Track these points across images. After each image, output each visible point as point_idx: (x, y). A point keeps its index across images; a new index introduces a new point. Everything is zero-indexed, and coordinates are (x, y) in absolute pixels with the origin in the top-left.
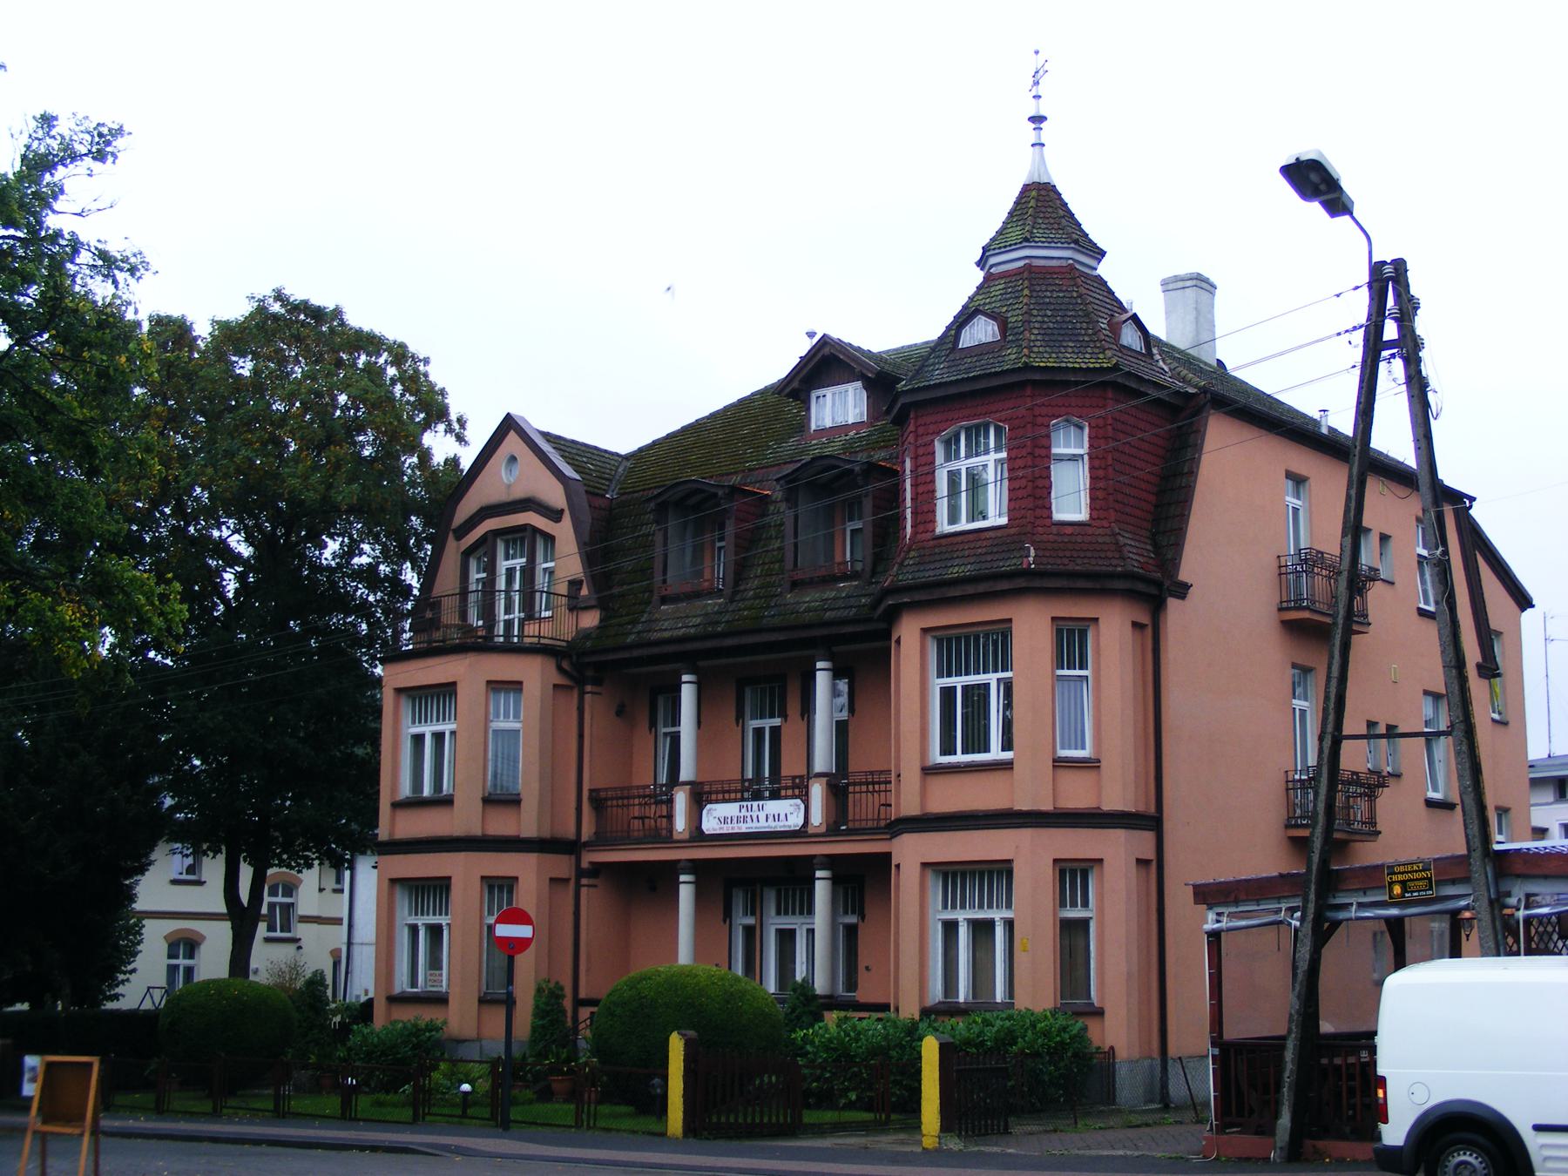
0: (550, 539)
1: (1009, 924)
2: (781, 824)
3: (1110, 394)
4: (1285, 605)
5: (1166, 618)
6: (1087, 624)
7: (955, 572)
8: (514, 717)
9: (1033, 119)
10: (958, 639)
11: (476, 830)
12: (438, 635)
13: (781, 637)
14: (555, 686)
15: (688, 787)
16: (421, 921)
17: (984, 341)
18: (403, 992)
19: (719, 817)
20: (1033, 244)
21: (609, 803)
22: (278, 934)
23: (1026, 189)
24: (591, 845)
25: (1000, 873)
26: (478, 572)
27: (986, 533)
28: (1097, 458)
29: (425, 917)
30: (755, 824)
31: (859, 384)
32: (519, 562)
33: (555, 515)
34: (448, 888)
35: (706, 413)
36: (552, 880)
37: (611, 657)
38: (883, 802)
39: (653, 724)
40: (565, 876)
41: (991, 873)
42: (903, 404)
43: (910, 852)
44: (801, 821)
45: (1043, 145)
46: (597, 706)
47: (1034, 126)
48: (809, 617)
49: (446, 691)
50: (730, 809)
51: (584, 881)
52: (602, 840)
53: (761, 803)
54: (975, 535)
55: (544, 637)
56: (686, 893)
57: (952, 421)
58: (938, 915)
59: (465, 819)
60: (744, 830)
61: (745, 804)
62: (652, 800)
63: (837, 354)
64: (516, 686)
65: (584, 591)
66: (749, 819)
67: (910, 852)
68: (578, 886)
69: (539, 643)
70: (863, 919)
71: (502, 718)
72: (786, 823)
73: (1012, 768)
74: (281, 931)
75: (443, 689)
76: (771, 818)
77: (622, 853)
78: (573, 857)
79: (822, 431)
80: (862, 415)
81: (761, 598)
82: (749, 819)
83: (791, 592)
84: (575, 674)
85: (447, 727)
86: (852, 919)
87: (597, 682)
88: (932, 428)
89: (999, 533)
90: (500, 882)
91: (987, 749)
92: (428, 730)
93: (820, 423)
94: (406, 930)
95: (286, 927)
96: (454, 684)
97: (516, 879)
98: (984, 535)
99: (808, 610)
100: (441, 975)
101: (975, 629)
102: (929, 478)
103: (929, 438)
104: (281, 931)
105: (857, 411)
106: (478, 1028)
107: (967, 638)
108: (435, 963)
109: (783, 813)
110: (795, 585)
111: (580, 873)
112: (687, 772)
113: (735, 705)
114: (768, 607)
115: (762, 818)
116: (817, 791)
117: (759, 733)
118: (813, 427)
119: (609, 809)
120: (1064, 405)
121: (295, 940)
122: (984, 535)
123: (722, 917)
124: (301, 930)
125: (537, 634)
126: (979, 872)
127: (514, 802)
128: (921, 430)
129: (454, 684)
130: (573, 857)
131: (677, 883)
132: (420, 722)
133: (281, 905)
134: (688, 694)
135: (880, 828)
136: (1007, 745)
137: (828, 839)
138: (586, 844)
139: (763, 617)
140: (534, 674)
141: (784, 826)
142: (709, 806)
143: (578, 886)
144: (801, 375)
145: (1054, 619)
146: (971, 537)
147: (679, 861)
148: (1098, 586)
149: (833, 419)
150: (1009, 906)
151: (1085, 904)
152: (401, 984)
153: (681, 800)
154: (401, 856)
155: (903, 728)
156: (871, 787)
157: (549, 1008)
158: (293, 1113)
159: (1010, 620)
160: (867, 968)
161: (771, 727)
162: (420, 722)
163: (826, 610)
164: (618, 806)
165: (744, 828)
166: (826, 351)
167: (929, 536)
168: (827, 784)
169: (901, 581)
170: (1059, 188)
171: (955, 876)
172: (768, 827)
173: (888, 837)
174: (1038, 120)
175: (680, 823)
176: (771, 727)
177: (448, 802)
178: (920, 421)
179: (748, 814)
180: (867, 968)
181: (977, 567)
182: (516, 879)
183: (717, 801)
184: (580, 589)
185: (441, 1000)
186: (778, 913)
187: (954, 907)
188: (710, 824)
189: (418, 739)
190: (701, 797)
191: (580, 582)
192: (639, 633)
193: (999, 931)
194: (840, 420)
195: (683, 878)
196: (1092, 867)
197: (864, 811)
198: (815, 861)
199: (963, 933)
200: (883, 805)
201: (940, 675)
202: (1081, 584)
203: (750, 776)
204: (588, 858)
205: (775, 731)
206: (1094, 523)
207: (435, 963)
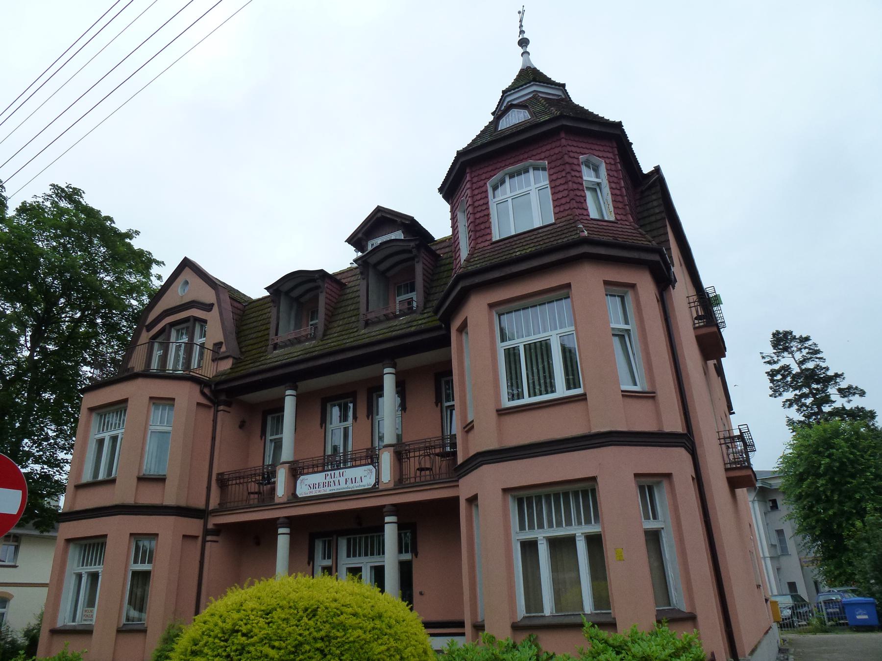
0: (204, 322)
2: (357, 484)
6: (626, 289)
11: (130, 500)
14: (198, 404)
16: (85, 570)
18: (64, 626)
21: (230, 483)
23: (522, 71)
24: (216, 512)
25: (585, 493)
29: (88, 567)
30: (337, 487)
32: (185, 339)
33: (208, 307)
34: (103, 545)
36: (185, 536)
39: (263, 433)
41: (566, 495)
42: (462, 162)
44: (372, 481)
46: (227, 420)
49: (120, 406)
50: (317, 478)
51: (209, 538)
52: (223, 509)
53: (341, 471)
56: (283, 541)
57: (496, 170)
60: (328, 492)
61: (329, 473)
64: (169, 401)
65: (223, 349)
66: (332, 484)
68: (204, 542)
70: (416, 556)
72: (361, 484)
77: (234, 516)
82: (332, 484)
83: (365, 328)
84: (212, 398)
85: (119, 432)
86: (407, 557)
87: (229, 404)
88: (483, 177)
91: (551, 388)
94: (74, 577)
103: (482, 183)
106: (114, 653)
108: (91, 603)
110: (367, 324)
111: (207, 532)
112: (287, 454)
115: (342, 480)
116: (386, 459)
119: (230, 487)
123: (307, 560)
126: (564, 493)
128: (475, 180)
131: (275, 535)
136: (572, 381)
142: (302, 477)
143: (204, 542)
147: (384, 506)
152: (64, 620)
154: (75, 522)
155: (415, 439)
160: (421, 593)
164: (236, 484)
165: (328, 491)
166: (379, 215)
175: (281, 491)
177: (110, 481)
178: (474, 174)
179: (332, 480)
180: (421, 593)
183: (308, 474)
184: (220, 348)
186: (348, 556)
187: (531, 527)
188: (303, 490)
189: (101, 442)
190: (296, 471)
191: (221, 343)
193: (581, 547)
195: (281, 531)
196: (659, 483)
198: (385, 510)
203: (330, 453)
204: (214, 521)
207: (91, 603)
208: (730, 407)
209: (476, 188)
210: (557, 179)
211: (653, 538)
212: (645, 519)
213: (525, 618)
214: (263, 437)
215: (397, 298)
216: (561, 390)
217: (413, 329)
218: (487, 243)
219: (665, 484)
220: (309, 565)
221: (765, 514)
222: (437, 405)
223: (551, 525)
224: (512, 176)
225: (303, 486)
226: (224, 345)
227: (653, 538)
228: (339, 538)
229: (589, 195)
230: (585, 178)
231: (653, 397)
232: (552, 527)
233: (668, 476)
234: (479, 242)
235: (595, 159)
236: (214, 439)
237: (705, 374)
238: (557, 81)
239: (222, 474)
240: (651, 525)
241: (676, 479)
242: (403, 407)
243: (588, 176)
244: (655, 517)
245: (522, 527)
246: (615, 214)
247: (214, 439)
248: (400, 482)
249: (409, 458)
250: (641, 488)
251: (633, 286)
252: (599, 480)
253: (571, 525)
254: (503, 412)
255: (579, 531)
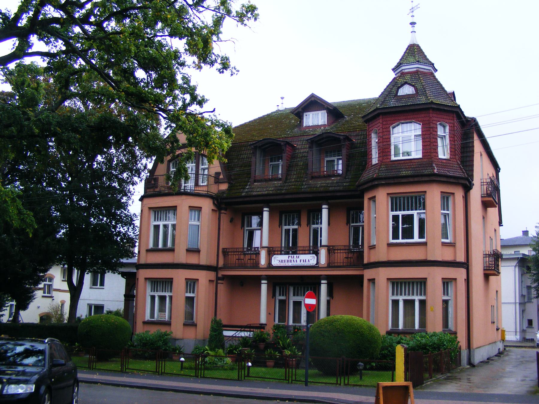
1: (171, 297)
3: (431, 111)
4: (483, 195)
5: (470, 196)
7: (404, 173)
8: (194, 220)
9: (411, 24)
10: (404, 198)
12: (157, 190)
13: (311, 196)
14: (212, 210)
15: (266, 249)
17: (408, 93)
19: (277, 260)
20: (420, 63)
21: (230, 253)
22: (46, 295)
25: (421, 283)
26: (173, 168)
27: (416, 160)
28: (452, 137)
31: (325, 111)
35: (248, 121)
37: (236, 200)
38: (249, 258)
39: (243, 226)
40: (213, 279)
43: (143, 274)
44: (315, 263)
45: (415, 32)
47: (411, 26)
48: (322, 189)
50: (285, 257)
51: (219, 282)
52: (226, 267)
53: (298, 255)
54: (404, 161)
55: (209, 192)
56: (264, 287)
58: (149, 293)
59: (181, 257)
61: (291, 255)
62: (242, 253)
63: (317, 100)
64: (199, 209)
65: (221, 177)
66: (292, 261)
67: (143, 274)
69: (208, 194)
71: (193, 220)
72: (309, 263)
73: (375, 248)
74: (47, 294)
75: (160, 209)
76: (302, 261)
78: (216, 272)
79: (309, 127)
80: (325, 122)
81: (298, 182)
87: (226, 210)
88: (389, 122)
89: (420, 161)
90: (160, 280)
91: (413, 238)
92: (161, 223)
93: (307, 124)
95: (49, 293)
96: (176, 206)
97: (172, 279)
98: (413, 161)
99: (321, 187)
100: (165, 314)
101: (408, 195)
102: (388, 140)
103: (388, 126)
104: (47, 294)
105: (323, 121)
107: (412, 198)
108: (162, 309)
109: (309, 259)
111: (218, 278)
113: (278, 221)
114: (303, 185)
115: (298, 260)
116: (323, 252)
117: (287, 231)
118: (304, 125)
119: (230, 256)
120: (441, 118)
121: (52, 297)
122: (413, 161)
123: (272, 296)
124: (54, 294)
125: (207, 190)
127: (198, 251)
129: (176, 206)
130: (216, 272)
131: (320, 284)
132: (158, 220)
133: (48, 285)
134: (325, 213)
135: (343, 266)
137: (328, 269)
138: (221, 268)
139: (302, 188)
140: (207, 205)
141: (308, 264)
142: (275, 256)
144: (302, 107)
145: (441, 192)
146: (403, 162)
147: (321, 275)
148: (457, 182)
149: (312, 123)
150: (171, 292)
151: (193, 292)
153: (263, 254)
156: (240, 253)
157: (218, 328)
158: (166, 373)
159: (425, 192)
161: (292, 229)
162: (158, 220)
163: (330, 187)
165: (290, 264)
166: (313, 99)
167: (388, 160)
168: (328, 249)
169: (380, 175)
170: (420, 45)
171: (156, 283)
172: (301, 264)
173: (363, 269)
174: (413, 24)
175: (263, 261)
176: (292, 229)
177: (172, 250)
179: (292, 259)
181: (414, 172)
182: (198, 280)
183: (278, 254)
185: (168, 324)
186: (294, 295)
189: (157, 227)
190: (271, 252)
192: (247, 192)
193: (168, 299)
194: (316, 123)
197: (336, 258)
198: (321, 277)
199: (157, 299)
200: (237, 259)
201: (392, 210)
202: (452, 180)
204: (221, 273)
205: (295, 231)
206: (450, 159)
208: (500, 223)
209: (384, 128)
210: (426, 134)
211: (446, 302)
212: (443, 295)
213: (391, 329)
214: (243, 228)
215: (325, 158)
216: (416, 239)
217: (341, 188)
218: (388, 160)
219: (453, 283)
220: (273, 298)
221: (522, 275)
222: (347, 225)
223: (405, 294)
224: (402, 123)
225: (276, 260)
226: (222, 174)
227: (446, 302)
228: (290, 287)
229: (439, 140)
230: (439, 133)
231: (454, 246)
232: (406, 295)
233: (455, 279)
234: (384, 158)
235: (443, 123)
236: (219, 229)
237: (483, 218)
238: (430, 60)
239: (223, 249)
240: (446, 298)
241: (458, 280)
242: (329, 224)
243: (440, 131)
244: (447, 295)
245: (393, 294)
246: (450, 155)
247: (219, 229)
248: (330, 265)
249: (335, 253)
250: (444, 283)
251: (453, 194)
252: (428, 279)
253: (414, 295)
254: (390, 245)
255: (417, 298)
